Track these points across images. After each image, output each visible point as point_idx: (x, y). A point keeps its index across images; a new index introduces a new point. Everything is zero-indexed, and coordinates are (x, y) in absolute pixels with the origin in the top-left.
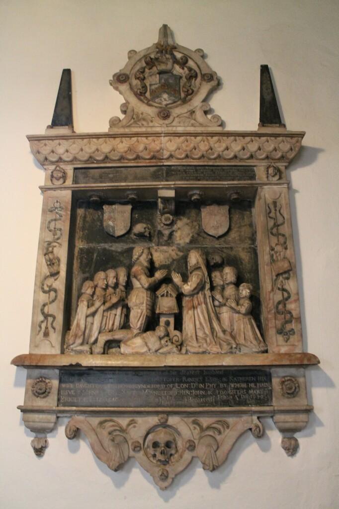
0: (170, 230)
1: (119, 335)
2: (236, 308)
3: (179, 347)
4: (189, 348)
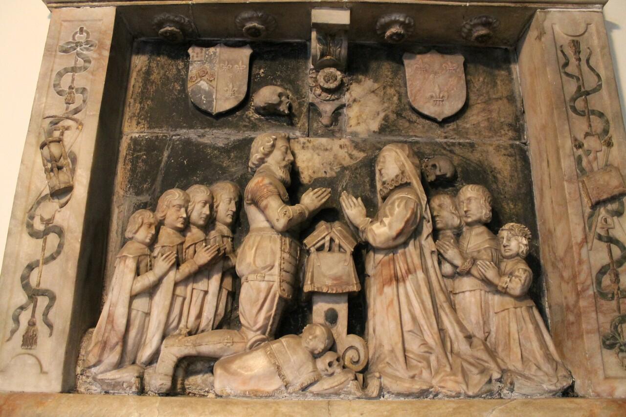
0: (337, 104)
1: (210, 344)
2: (496, 281)
3: (360, 377)
4: (386, 381)
